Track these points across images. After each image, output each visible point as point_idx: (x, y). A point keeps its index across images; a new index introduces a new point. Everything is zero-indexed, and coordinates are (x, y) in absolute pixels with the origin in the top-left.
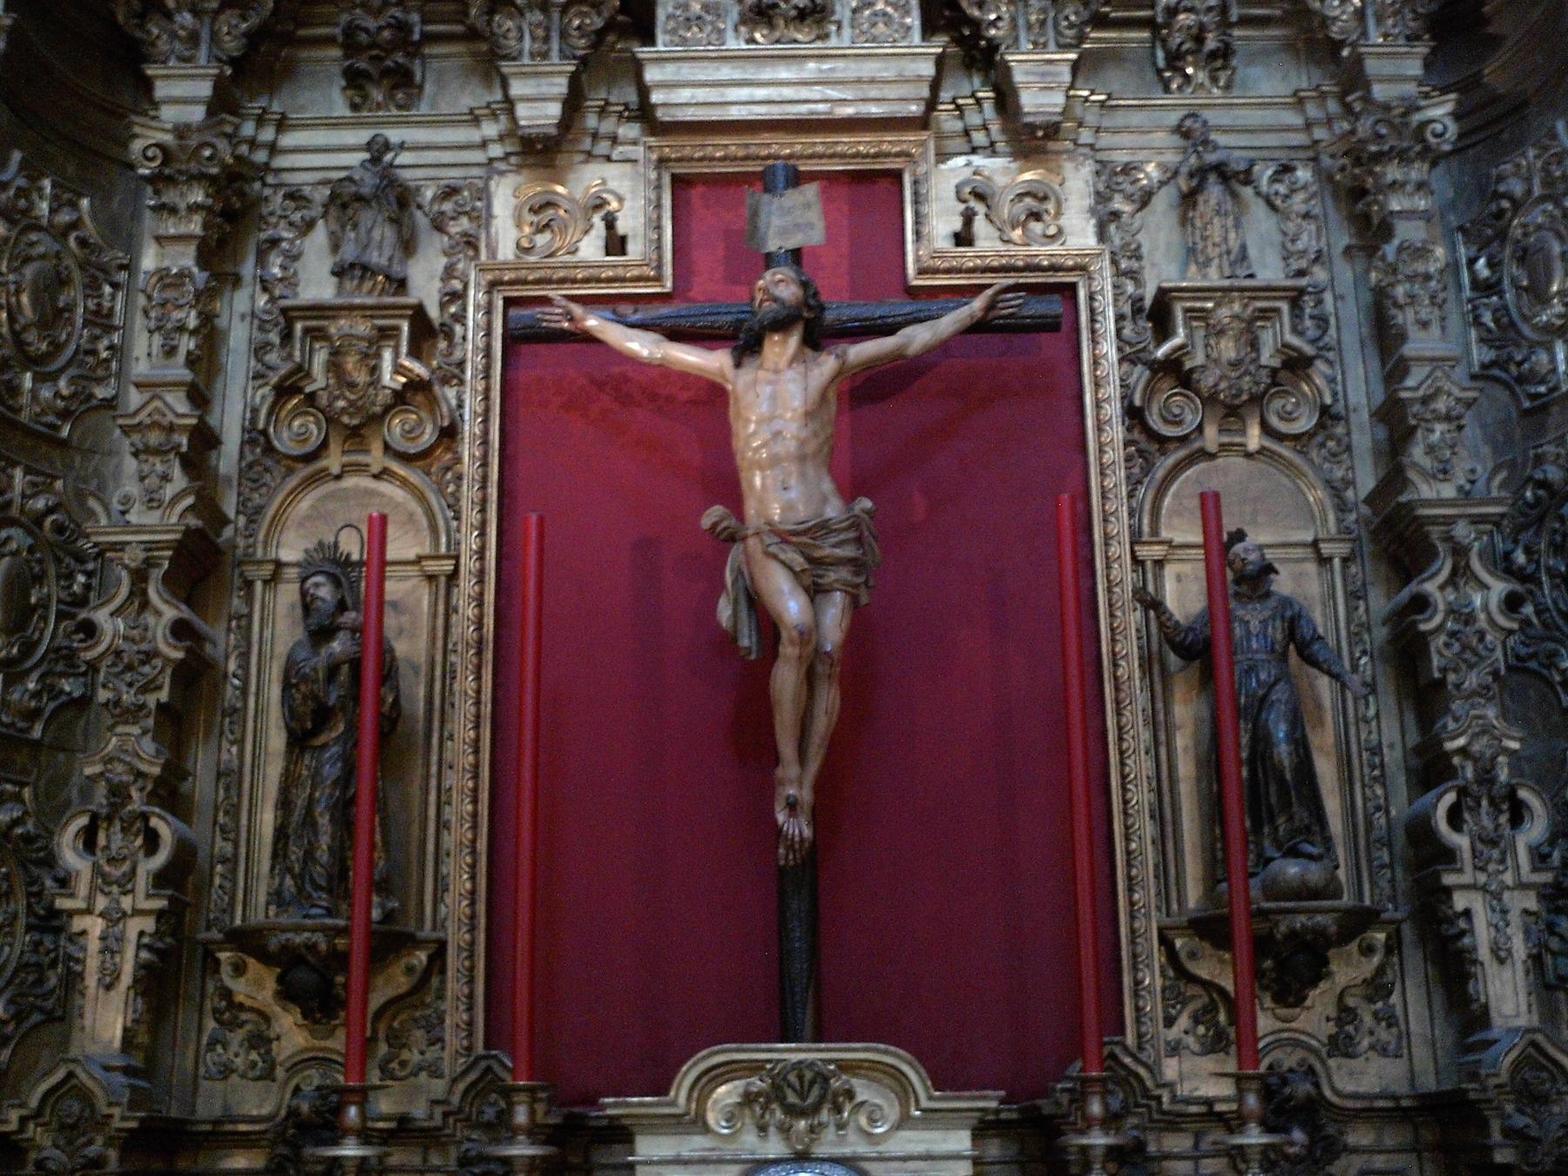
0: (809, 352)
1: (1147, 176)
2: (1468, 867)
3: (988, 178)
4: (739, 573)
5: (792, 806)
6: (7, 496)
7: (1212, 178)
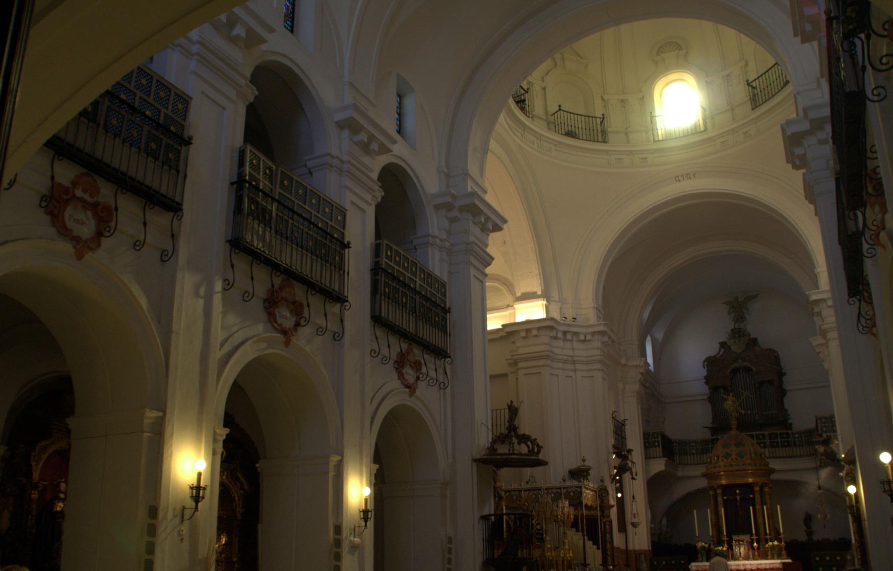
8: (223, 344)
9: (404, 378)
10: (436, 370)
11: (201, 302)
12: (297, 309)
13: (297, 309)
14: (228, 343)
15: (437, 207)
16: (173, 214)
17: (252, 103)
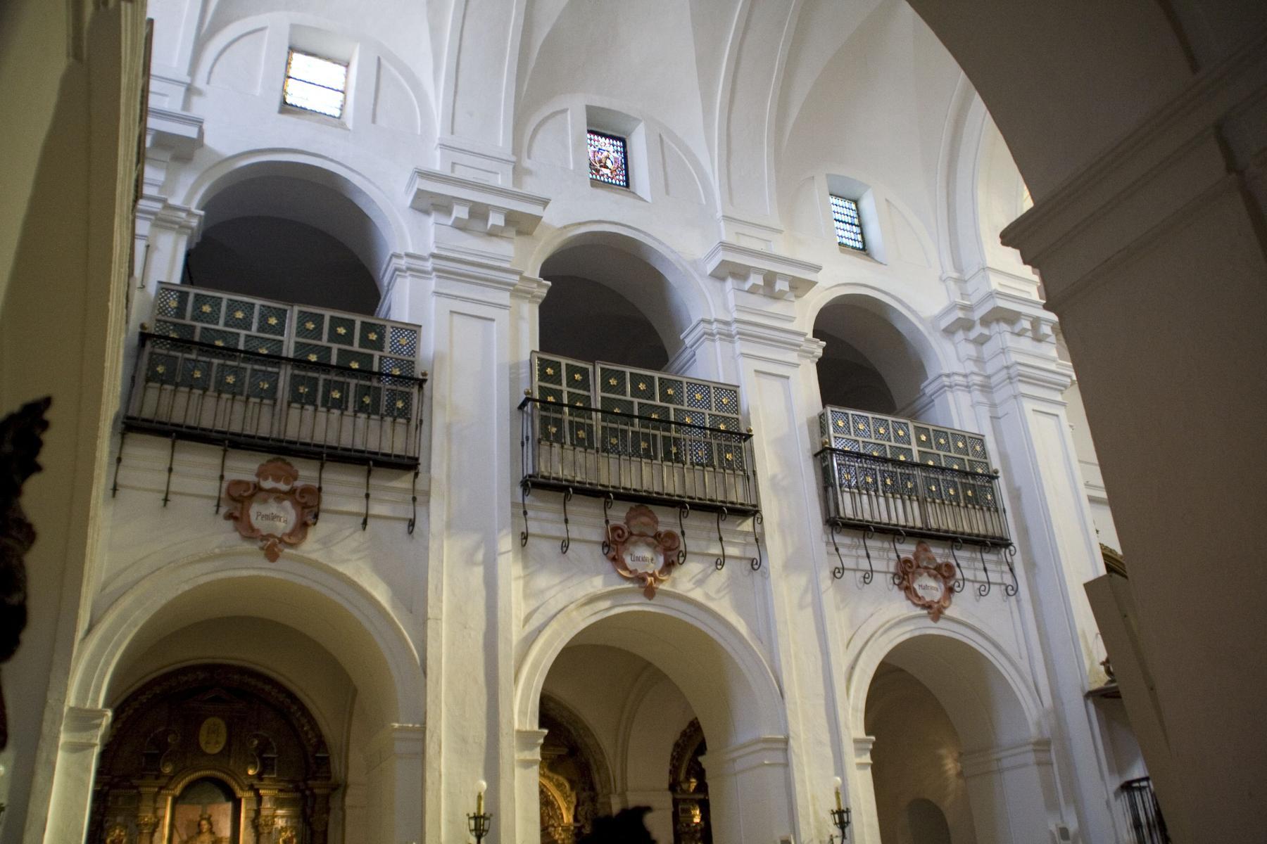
0: (273, 799)
1: (304, 390)
2: (686, 404)
6: (98, 721)
7: (943, 279)
8: (527, 619)
9: (917, 595)
10: (985, 570)
11: (479, 571)
12: (945, 573)
13: (945, 573)
14: (536, 615)
15: (949, 332)
16: (752, 518)
17: (822, 357)
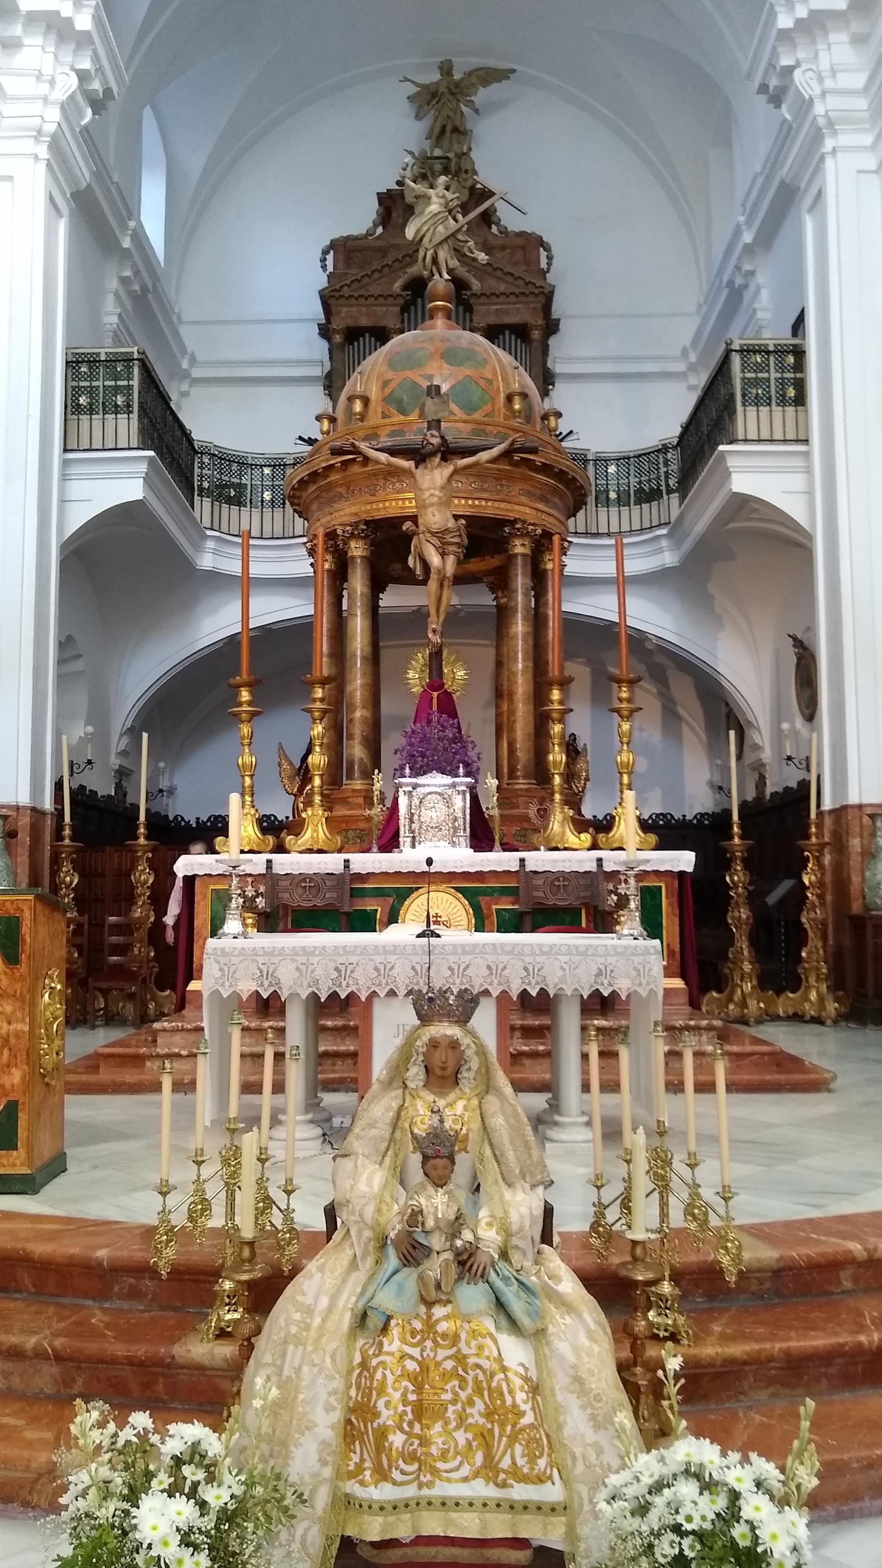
3: (432, 469)
4: (416, 547)
5: (434, 631)
